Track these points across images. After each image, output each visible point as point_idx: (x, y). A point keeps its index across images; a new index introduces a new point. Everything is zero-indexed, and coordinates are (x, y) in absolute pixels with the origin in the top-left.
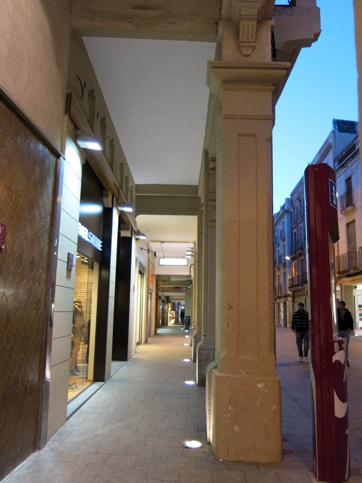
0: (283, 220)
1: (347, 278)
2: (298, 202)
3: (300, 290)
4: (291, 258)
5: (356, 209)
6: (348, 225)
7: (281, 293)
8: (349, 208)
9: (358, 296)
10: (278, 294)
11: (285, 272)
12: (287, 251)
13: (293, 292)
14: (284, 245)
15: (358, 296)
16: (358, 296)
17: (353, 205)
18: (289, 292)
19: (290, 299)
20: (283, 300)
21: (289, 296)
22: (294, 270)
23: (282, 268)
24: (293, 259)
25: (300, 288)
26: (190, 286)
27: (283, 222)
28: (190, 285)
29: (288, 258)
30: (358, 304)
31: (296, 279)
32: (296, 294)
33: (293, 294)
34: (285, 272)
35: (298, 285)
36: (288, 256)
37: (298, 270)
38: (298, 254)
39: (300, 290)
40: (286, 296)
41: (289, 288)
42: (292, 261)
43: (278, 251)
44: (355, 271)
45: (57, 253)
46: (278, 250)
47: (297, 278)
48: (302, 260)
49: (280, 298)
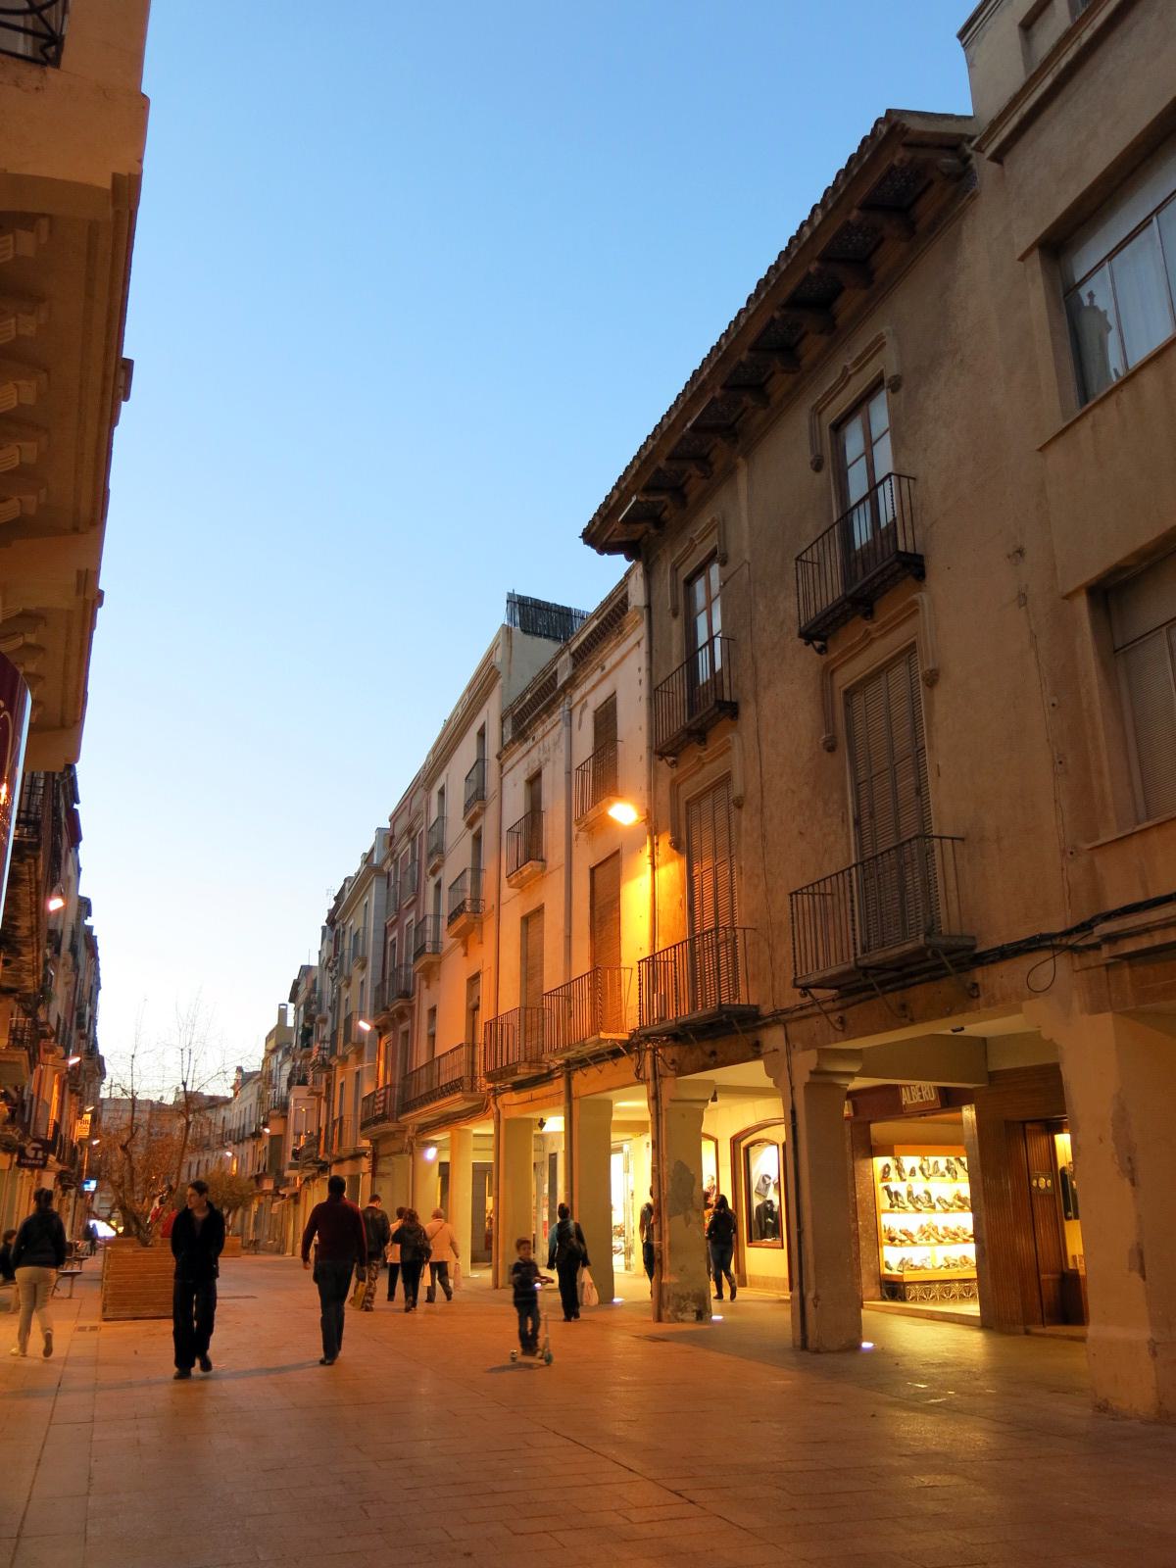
1: (513, 1093)
2: (409, 841)
5: (549, 869)
6: (526, 920)
8: (528, 869)
13: (375, 1142)
17: (542, 860)
24: (381, 1030)
32: (383, 1149)
44: (533, 1071)
48: (406, 1033)
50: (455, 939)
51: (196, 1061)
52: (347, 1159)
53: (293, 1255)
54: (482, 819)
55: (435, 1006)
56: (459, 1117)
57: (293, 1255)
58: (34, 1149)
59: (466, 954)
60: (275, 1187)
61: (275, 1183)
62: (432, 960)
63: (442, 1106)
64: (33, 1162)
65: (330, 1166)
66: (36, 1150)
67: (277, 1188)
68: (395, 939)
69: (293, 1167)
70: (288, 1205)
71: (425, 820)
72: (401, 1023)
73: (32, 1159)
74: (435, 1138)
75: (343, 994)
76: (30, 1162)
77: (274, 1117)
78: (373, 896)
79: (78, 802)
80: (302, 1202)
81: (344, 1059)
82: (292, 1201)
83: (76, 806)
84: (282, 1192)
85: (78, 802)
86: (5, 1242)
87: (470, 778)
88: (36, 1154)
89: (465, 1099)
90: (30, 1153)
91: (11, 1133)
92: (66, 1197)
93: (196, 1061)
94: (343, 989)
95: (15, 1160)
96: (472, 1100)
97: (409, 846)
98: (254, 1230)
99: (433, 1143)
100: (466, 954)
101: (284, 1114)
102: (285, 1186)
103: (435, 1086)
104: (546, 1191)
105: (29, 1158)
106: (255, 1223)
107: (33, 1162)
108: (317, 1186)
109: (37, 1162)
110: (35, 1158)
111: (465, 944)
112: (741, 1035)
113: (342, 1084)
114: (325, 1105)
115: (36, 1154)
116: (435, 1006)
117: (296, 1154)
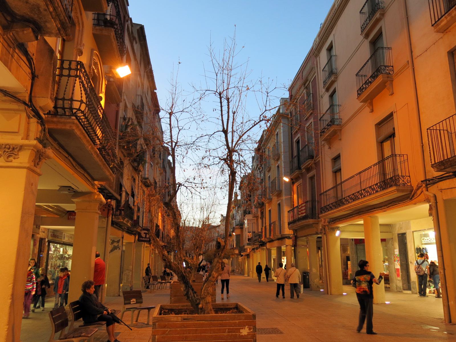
0: (278, 130)
2: (304, 89)
3: (309, 226)
4: (292, 179)
7: (274, 233)
9: (413, 232)
10: (270, 235)
11: (279, 204)
12: (368, 28)
13: (295, 231)
14: (278, 167)
15: (414, 232)
16: (413, 232)
18: (288, 231)
19: (289, 242)
20: (276, 243)
21: (289, 238)
22: (295, 196)
23: (275, 199)
24: (293, 181)
25: (311, 221)
26: (73, 202)
27: (277, 134)
28: (74, 200)
29: (286, 179)
30: (416, 247)
31: (303, 208)
32: (299, 234)
33: (294, 234)
34: (279, 204)
35: (305, 218)
36: (286, 176)
37: (305, 195)
38: (304, 168)
39: (309, 226)
40: (282, 238)
41: (289, 224)
42: (293, 183)
43: (269, 177)
45: (309, 276)
46: (268, 176)
47: (304, 209)
48: (312, 178)
49: (271, 241)
50: (363, 103)
51: (234, 113)
52: (275, 240)
53: (248, 276)
54: (336, 83)
55: (339, 154)
56: (374, 208)
57: (248, 276)
58: (144, 233)
59: (372, 111)
60: (239, 252)
61: (239, 250)
62: (336, 129)
63: (366, 201)
64: (145, 239)
65: (266, 244)
66: (146, 234)
67: (240, 252)
68: (299, 137)
69: (248, 244)
70: (244, 258)
71: (316, 71)
72: (308, 174)
73: (144, 238)
74: (341, 225)
75: (266, 175)
76: (143, 239)
77: (237, 228)
78: (282, 130)
79: (156, 89)
80: (251, 257)
81: (270, 200)
82: (246, 257)
83: (155, 91)
84: (242, 254)
85: (156, 89)
86: (84, 291)
87: (363, 11)
88: (146, 236)
89: (398, 190)
90: (144, 236)
91: (122, 220)
92: (169, 255)
93: (234, 113)
94: (266, 173)
95: (137, 238)
96: (402, 191)
97: (305, 91)
98: (231, 266)
99: (338, 228)
100: (372, 111)
101: (242, 227)
102: (244, 252)
103: (340, 198)
104: (397, 252)
105: (142, 237)
106: (231, 264)
107: (145, 239)
108: (259, 251)
109: (146, 239)
110: (146, 237)
111: (371, 104)
112: (58, 295)
113: (270, 211)
114: (261, 220)
115: (146, 236)
116: (339, 154)
117: (249, 240)
